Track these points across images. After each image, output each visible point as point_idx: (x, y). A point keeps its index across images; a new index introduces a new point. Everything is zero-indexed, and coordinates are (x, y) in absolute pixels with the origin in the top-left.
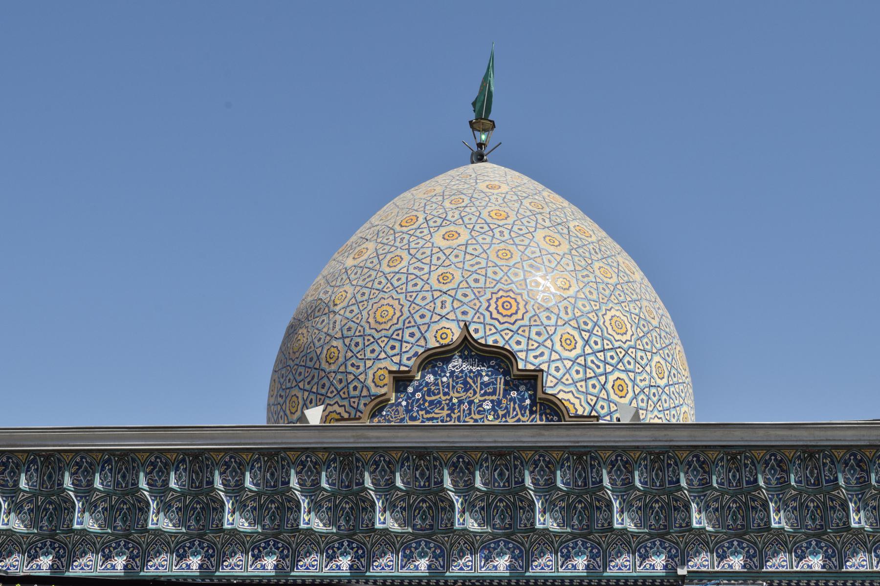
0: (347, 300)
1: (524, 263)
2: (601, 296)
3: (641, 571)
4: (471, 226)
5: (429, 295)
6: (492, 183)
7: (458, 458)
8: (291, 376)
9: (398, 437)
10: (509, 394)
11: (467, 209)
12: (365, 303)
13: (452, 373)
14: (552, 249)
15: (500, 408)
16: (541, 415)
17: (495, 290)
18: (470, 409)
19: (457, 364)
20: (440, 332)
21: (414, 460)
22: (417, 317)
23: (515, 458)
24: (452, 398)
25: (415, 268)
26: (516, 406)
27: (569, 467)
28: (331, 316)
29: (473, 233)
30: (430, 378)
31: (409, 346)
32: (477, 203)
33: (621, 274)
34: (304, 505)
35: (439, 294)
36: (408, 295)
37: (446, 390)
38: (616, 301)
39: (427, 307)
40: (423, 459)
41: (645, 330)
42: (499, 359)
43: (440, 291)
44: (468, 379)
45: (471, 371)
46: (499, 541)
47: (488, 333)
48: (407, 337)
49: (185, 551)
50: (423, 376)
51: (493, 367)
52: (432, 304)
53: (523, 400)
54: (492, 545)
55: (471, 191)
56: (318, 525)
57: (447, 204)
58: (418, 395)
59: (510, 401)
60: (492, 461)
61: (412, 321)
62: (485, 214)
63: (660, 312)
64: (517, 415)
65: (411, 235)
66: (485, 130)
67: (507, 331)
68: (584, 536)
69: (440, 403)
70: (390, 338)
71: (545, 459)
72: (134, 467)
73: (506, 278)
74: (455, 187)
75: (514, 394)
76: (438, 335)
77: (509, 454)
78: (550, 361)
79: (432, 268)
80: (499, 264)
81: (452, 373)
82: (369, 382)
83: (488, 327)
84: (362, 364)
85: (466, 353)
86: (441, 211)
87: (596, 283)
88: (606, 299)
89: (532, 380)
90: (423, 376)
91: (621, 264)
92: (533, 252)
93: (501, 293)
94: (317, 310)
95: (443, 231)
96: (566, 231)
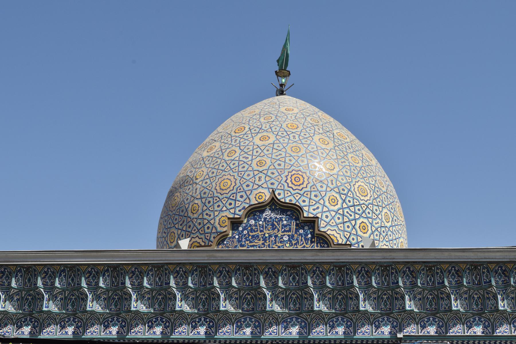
0: (203, 176)
1: (308, 154)
2: (352, 174)
3: (376, 335)
4: (276, 133)
5: (251, 173)
6: (289, 107)
7: (269, 269)
8: (170, 221)
9: (233, 257)
10: (299, 232)
11: (274, 123)
12: (214, 178)
13: (265, 219)
14: (324, 146)
15: (293, 240)
16: (317, 244)
17: (290, 170)
18: (275, 240)
19: (268, 214)
20: (258, 195)
21: (243, 270)
22: (244, 186)
23: (302, 269)
24: (265, 234)
25: (243, 157)
26: (303, 238)
27: (334, 274)
28: (194, 185)
29: (277, 137)
30: (252, 222)
31: (240, 203)
32: (280, 119)
33: (364, 161)
34: (179, 296)
35: (257, 172)
36: (240, 173)
37: (262, 229)
38: (361, 177)
39: (250, 180)
40: (248, 269)
41: (378, 194)
42: (293, 211)
43: (258, 171)
44: (275, 223)
45: (276, 218)
46: (293, 318)
47: (286, 195)
48: (239, 198)
49: (108, 323)
50: (248, 221)
51: (289, 215)
52: (253, 179)
53: (306, 235)
54: (289, 320)
55: (276, 112)
56: (186, 308)
57: (262, 120)
58: (245, 232)
59: (299, 235)
60: (289, 271)
61: (242, 188)
62: (284, 126)
63: (387, 183)
64: (303, 243)
65: (241, 138)
66: (284, 77)
67: (297, 195)
68: (343, 315)
69: (258, 236)
70: (229, 198)
71: (319, 270)
72: (78, 274)
73: (297, 163)
74: (267, 110)
75: (301, 231)
76: (257, 197)
77: (299, 267)
78: (322, 212)
79: (254, 158)
80: (293, 155)
81: (265, 219)
82: (217, 224)
83: (286, 192)
84: (212, 214)
85: (273, 207)
86: (259, 124)
87: (350, 166)
88: (355, 176)
89: (312, 223)
90: (248, 221)
91: (364, 155)
92: (313, 148)
93: (294, 172)
94: (186, 182)
95: (260, 135)
96: (332, 136)
